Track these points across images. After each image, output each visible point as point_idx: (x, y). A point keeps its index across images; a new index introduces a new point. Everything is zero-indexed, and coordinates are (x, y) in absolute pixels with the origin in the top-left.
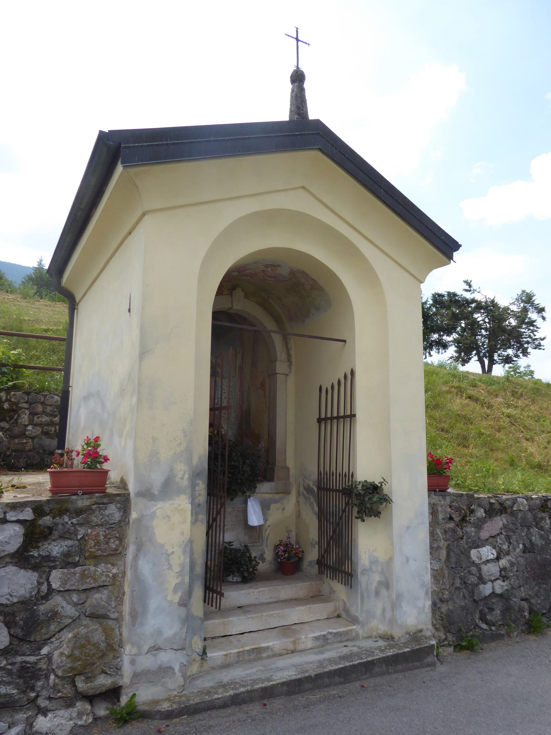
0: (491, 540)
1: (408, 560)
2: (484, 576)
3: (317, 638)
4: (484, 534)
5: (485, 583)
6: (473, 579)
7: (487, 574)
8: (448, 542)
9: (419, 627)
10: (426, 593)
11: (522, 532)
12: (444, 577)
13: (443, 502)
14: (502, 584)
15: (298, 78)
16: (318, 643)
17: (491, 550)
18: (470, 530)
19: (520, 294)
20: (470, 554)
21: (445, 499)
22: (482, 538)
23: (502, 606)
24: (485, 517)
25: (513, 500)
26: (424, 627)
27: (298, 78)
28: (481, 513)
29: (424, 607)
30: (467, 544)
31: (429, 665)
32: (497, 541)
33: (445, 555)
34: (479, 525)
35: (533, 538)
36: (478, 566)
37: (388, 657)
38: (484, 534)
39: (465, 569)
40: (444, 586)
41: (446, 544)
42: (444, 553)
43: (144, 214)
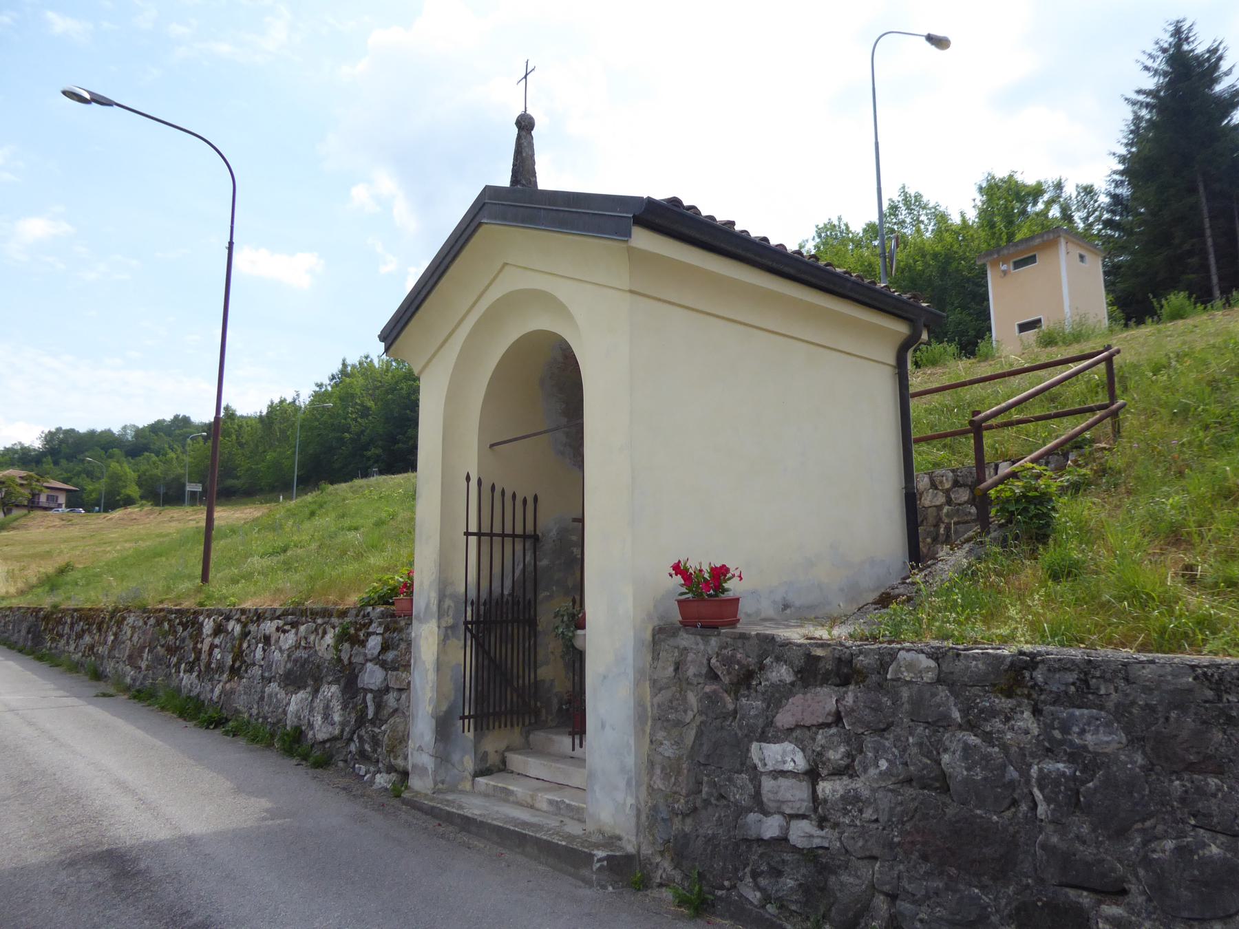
0: (798, 733)
1: (603, 726)
2: (765, 800)
3: (551, 802)
4: (784, 718)
5: (766, 813)
6: (740, 796)
7: (771, 796)
8: (704, 718)
9: (617, 832)
10: (628, 783)
11: (911, 734)
12: (679, 773)
13: (702, 647)
14: (816, 832)
15: (525, 125)
16: (551, 809)
17: (793, 752)
18: (753, 705)
19: (821, 226)
20: (748, 750)
21: (707, 643)
22: (779, 724)
23: (804, 876)
24: (793, 684)
25: (880, 654)
26: (623, 834)
27: (525, 125)
28: (782, 673)
29: (624, 804)
30: (741, 727)
31: (584, 880)
32: (814, 739)
33: (692, 738)
34: (777, 697)
35: (946, 758)
36: (755, 774)
37: (540, 839)
38: (784, 718)
39: (723, 773)
40: (678, 789)
41: (699, 719)
42: (691, 735)
43: (503, 267)
